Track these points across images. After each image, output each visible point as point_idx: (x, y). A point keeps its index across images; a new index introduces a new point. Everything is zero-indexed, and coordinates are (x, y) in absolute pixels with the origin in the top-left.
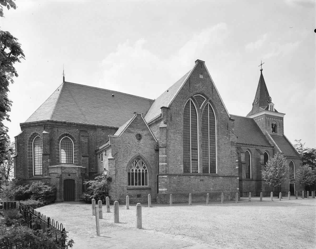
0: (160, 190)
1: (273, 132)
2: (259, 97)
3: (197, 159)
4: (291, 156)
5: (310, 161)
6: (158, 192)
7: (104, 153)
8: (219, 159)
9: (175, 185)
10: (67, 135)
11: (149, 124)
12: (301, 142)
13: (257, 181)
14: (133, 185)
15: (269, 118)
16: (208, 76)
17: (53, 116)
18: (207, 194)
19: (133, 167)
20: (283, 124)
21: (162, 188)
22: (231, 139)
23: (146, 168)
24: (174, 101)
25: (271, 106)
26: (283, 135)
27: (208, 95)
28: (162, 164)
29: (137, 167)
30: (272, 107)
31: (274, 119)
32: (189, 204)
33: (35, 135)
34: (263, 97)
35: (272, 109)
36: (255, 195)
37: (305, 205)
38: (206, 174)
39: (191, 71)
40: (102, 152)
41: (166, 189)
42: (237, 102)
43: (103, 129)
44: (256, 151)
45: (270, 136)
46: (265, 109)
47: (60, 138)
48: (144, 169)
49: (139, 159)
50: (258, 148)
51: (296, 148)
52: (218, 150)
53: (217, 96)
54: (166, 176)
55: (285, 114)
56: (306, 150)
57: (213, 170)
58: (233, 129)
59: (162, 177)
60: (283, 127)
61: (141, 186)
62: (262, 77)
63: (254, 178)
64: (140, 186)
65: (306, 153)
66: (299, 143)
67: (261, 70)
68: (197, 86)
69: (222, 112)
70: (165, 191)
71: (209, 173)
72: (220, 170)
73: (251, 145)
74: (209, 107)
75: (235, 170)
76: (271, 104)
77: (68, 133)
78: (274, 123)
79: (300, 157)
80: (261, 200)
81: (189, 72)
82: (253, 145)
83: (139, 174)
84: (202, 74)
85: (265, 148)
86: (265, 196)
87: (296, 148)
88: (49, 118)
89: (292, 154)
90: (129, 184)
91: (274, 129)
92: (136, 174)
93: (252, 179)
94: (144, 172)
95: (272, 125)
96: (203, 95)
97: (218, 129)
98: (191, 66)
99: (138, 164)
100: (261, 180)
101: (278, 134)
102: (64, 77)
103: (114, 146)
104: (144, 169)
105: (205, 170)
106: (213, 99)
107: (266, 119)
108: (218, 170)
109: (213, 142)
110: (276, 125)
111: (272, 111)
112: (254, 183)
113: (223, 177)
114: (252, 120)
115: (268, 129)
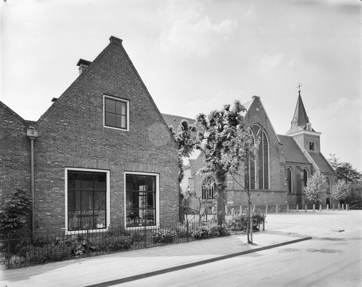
1: (310, 150)
2: (298, 117)
4: (327, 173)
5: (344, 175)
8: (271, 177)
9: (238, 199)
12: (335, 156)
13: (297, 195)
15: (307, 137)
16: (262, 109)
18: (267, 206)
20: (319, 142)
21: (229, 201)
22: (280, 160)
25: (308, 126)
26: (320, 152)
27: (262, 125)
28: (230, 182)
29: (208, 184)
30: (310, 126)
31: (312, 138)
32: (277, 213)
34: (302, 117)
35: (310, 129)
36: (112, 212)
37: (341, 214)
38: (261, 190)
41: (233, 203)
42: (281, 124)
44: (296, 168)
45: (308, 154)
46: (304, 129)
50: (298, 165)
51: (330, 162)
52: (271, 170)
54: (233, 192)
56: (339, 164)
58: (282, 152)
59: (230, 192)
60: (319, 145)
62: (300, 97)
63: (295, 193)
65: (340, 168)
66: (334, 158)
67: (299, 92)
68: (255, 117)
69: (273, 138)
72: (272, 186)
73: (292, 162)
74: (264, 136)
75: (284, 186)
76: (309, 124)
78: (312, 141)
79: (335, 173)
80: (306, 211)
82: (294, 163)
84: (258, 107)
85: (305, 165)
86: (308, 209)
87: (329, 162)
89: (328, 171)
91: (311, 147)
93: (293, 193)
95: (310, 143)
96: (259, 124)
97: (270, 152)
98: (252, 100)
101: (315, 151)
103: (193, 168)
106: (266, 127)
107: (304, 138)
108: (271, 187)
110: (313, 144)
111: (310, 130)
112: (294, 197)
113: (275, 192)
114: (291, 138)
115: (306, 147)
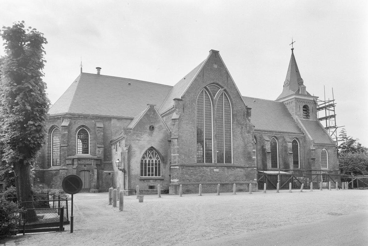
0: (171, 180)
3: (211, 149)
6: (170, 181)
7: (118, 144)
10: (83, 126)
11: (163, 115)
14: (85, 153)
17: (70, 108)
19: (153, 158)
23: (159, 158)
24: (188, 92)
33: (53, 127)
39: (205, 60)
40: (116, 143)
43: (118, 120)
47: (76, 131)
48: (158, 159)
49: (152, 150)
53: (232, 85)
55: (318, 97)
57: (229, 160)
61: (154, 176)
64: (156, 177)
67: (292, 49)
70: (177, 181)
71: (224, 163)
76: (302, 86)
77: (84, 124)
81: (203, 62)
83: (146, 164)
88: (67, 111)
90: (142, 175)
92: (156, 164)
94: (158, 162)
98: (205, 56)
99: (151, 155)
100: (311, 171)
102: (81, 68)
104: (158, 159)
105: (220, 160)
109: (228, 132)
111: (304, 94)
